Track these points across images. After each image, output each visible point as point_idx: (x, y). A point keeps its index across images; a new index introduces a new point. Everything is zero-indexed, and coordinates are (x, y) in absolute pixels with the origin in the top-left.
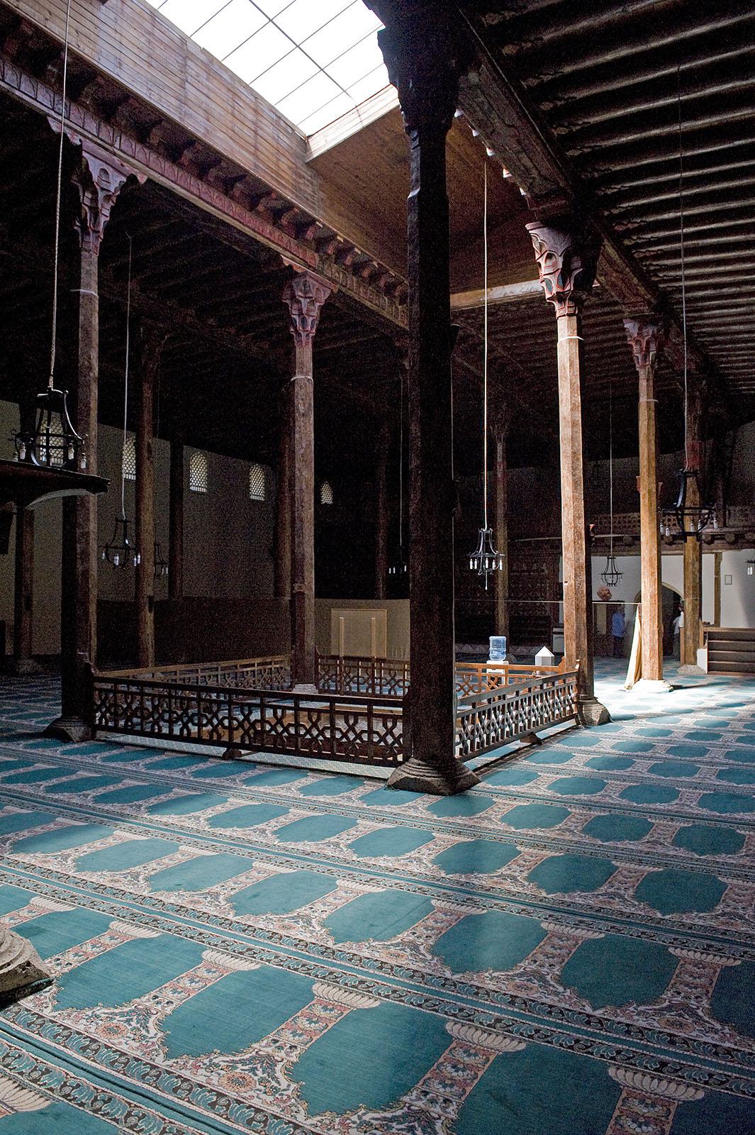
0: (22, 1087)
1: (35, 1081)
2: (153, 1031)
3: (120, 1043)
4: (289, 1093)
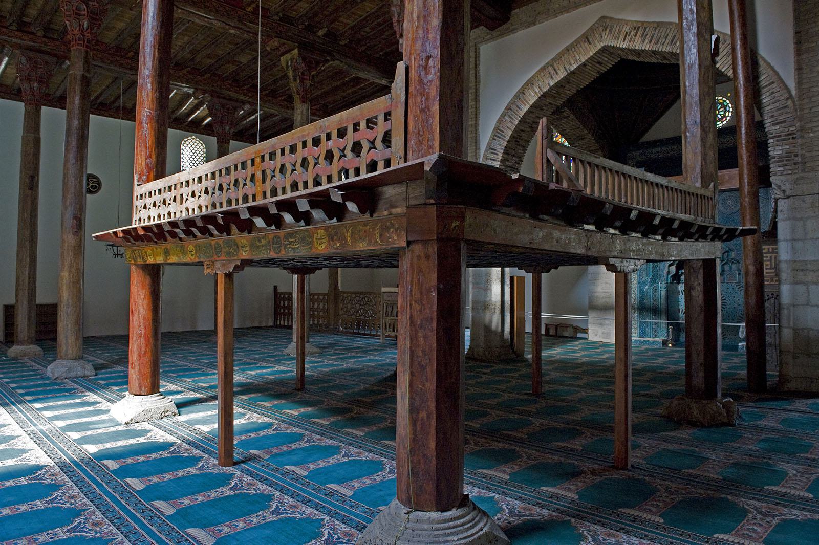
0: (293, 471)
1: (331, 492)
2: (326, 532)
3: (345, 528)
4: (326, 527)
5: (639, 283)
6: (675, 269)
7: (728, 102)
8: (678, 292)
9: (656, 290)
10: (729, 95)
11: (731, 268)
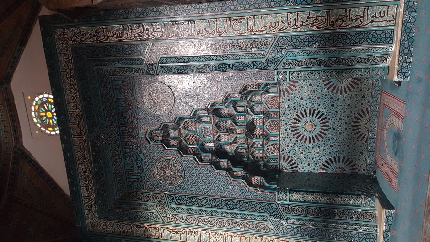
5: (277, 235)
6: (256, 177)
7: (37, 99)
8: (293, 172)
9: (289, 209)
10: (29, 97)
11: (258, 103)
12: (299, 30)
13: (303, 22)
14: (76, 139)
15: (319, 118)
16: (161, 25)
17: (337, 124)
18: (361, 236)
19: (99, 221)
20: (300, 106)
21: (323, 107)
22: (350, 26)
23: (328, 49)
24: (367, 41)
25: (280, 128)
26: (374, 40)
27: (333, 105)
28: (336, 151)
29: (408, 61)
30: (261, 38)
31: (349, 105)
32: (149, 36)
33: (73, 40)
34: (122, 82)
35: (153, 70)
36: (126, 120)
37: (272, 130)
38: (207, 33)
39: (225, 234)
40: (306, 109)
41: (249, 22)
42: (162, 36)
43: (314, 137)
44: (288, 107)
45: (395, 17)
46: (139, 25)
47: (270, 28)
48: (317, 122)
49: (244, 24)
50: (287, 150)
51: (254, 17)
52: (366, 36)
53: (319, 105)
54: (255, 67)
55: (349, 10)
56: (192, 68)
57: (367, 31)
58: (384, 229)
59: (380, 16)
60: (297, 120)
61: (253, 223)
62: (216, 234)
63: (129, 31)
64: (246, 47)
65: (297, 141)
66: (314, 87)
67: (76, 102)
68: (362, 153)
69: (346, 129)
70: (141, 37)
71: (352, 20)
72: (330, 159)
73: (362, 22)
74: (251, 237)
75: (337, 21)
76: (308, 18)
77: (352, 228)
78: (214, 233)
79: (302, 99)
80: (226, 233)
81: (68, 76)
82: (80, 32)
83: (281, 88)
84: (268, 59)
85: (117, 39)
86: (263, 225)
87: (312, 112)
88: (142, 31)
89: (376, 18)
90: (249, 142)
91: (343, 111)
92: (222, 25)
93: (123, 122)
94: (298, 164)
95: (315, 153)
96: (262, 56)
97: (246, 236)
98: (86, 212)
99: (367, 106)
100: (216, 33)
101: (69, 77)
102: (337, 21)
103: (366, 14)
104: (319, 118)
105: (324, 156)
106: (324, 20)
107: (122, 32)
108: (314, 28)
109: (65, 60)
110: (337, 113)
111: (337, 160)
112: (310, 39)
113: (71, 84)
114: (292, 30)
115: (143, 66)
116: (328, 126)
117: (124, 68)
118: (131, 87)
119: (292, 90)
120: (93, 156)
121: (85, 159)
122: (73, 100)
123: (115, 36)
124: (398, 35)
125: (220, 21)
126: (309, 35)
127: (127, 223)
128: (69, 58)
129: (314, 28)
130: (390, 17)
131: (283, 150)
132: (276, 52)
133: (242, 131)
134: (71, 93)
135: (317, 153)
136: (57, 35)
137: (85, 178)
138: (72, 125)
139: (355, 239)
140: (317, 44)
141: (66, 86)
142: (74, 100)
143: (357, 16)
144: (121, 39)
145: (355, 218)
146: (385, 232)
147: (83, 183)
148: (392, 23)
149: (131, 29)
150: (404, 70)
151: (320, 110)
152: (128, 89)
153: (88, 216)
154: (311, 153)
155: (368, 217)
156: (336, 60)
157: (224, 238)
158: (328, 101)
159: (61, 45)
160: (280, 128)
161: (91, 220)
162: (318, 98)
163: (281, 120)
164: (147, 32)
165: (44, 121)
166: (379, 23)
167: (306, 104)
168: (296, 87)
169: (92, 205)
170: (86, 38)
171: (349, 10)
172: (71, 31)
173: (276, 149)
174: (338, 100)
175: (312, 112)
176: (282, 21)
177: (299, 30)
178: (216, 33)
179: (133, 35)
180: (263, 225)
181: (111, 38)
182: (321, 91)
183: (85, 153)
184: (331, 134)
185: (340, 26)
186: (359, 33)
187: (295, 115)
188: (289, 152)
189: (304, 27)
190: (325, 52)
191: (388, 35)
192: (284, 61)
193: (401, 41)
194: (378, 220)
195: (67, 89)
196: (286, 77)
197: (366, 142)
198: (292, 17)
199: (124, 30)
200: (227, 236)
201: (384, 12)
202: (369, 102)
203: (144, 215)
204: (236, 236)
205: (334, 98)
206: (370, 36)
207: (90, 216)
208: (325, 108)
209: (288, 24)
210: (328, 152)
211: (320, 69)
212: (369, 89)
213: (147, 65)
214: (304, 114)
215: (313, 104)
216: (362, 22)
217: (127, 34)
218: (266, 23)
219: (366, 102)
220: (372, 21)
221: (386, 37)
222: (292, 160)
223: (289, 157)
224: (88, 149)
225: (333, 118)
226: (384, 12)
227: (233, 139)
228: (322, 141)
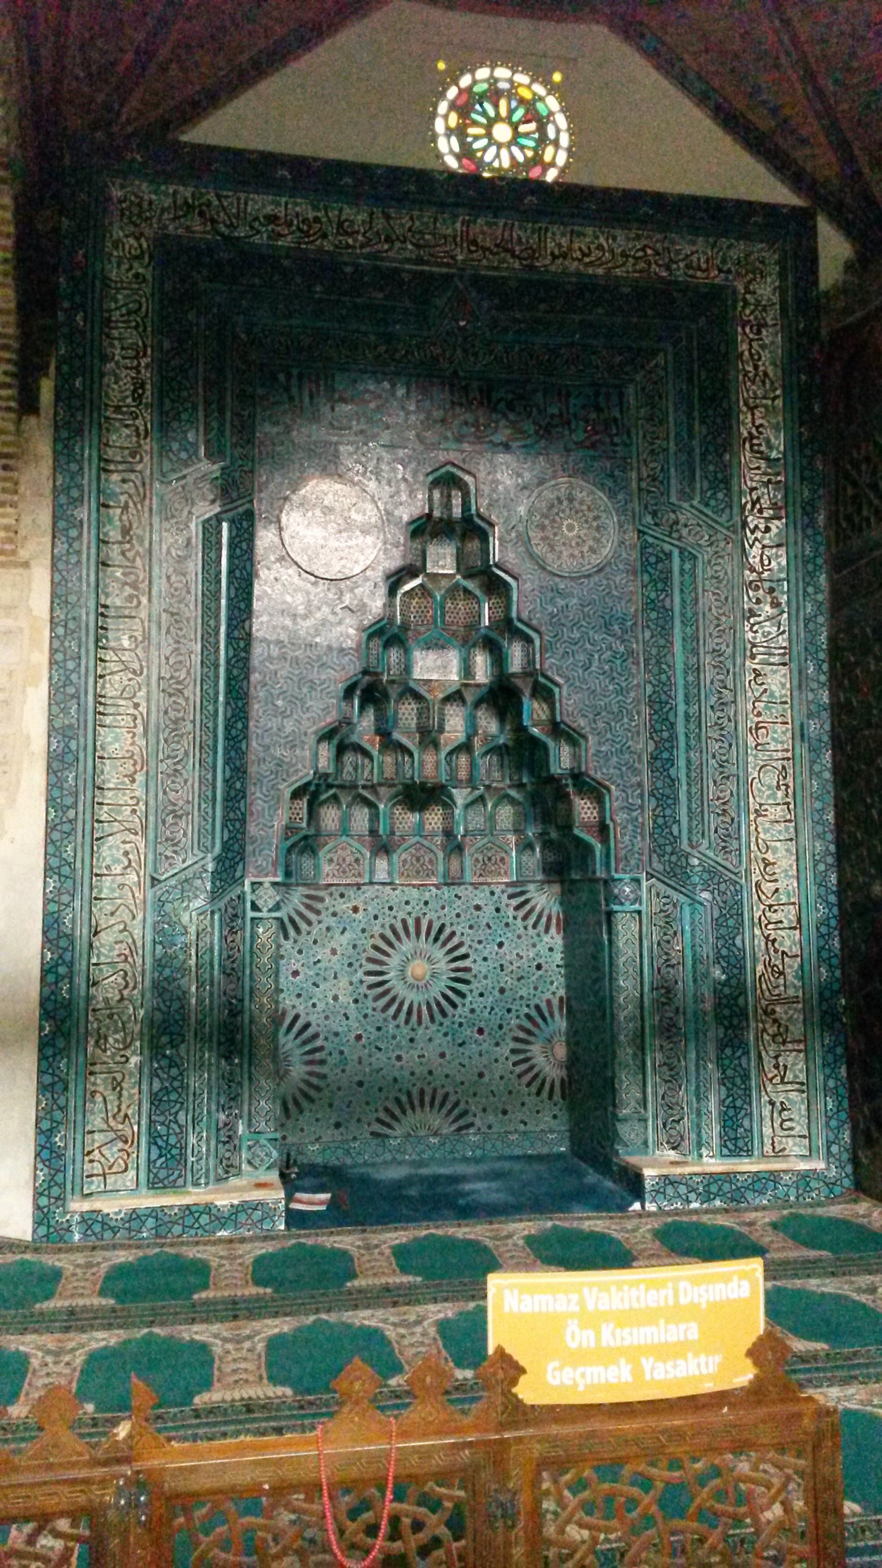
12: (757, 932)
13: (774, 940)
14: (458, 225)
15: (445, 996)
16: (780, 570)
17: (425, 1051)
18: (173, 1140)
19: (147, 231)
20: (480, 942)
21: (474, 1006)
22: (763, 1053)
23: (708, 1006)
24: (160, 1156)
25: (414, 886)
26: (731, 1112)
27: (481, 1031)
28: (342, 1053)
29: (692, 1196)
30: (739, 839)
31: (481, 1075)
32: (752, 532)
33: (748, 296)
34: (615, 420)
35: (656, 524)
36: (502, 405)
37: (405, 861)
38: (757, 694)
39: (136, 706)
40: (471, 959)
41: (779, 808)
42: (752, 570)
43: (386, 986)
44: (478, 908)
45: (780, 1154)
46: (780, 508)
47: (764, 859)
48: (435, 992)
49: (773, 796)
50: (343, 906)
51: (790, 821)
52: (740, 1092)
53: (481, 995)
54: (660, 821)
55: (802, 1047)
56: (662, 642)
57: (750, 1096)
58: (218, 1203)
59: (783, 1121)
60: (438, 935)
61: (188, 802)
62: (134, 672)
63: (765, 474)
64: (719, 798)
65: (372, 936)
66: (534, 978)
67: (574, 259)
68: (338, 1125)
69: (412, 1074)
70: (749, 506)
71: (776, 1057)
72: (316, 1036)
73: (771, 1080)
74: (137, 794)
75: (775, 1021)
76: (783, 952)
77: (198, 1111)
78: (136, 666)
79: (501, 945)
80: (143, 709)
81: (649, 252)
82: (766, 325)
83: (531, 887)
84: (687, 856)
85: (745, 434)
86: (185, 835)
87: (461, 977)
88: (765, 515)
89: (780, 1113)
90: (382, 790)
91: (466, 1062)
92: (773, 739)
93: (495, 396)
94: (295, 941)
95: (334, 992)
96: (695, 839)
97: (140, 778)
98: (186, 192)
99: (478, 1122)
100: (756, 719)
101: (646, 255)
102: (775, 1021)
103: (789, 1087)
104: (445, 996)
105: (327, 1018)
106: (777, 992)
107: (762, 453)
108: (760, 968)
109: (694, 257)
110: (460, 1045)
111: (314, 1056)
112: (734, 961)
113: (627, 256)
114: (757, 915)
115: (673, 500)
116: (420, 1022)
117: (667, 439)
118: (603, 443)
119: (525, 918)
120: (397, 271)
121: (388, 239)
122: (580, 249)
123: (754, 431)
124: (747, 1165)
125: (784, 733)
126: (744, 958)
127: (149, 342)
128: (700, 269)
129: (760, 968)
130: (780, 1142)
131: (342, 896)
132: (706, 876)
133: (429, 770)
134: (600, 247)
135: (335, 998)
136: (762, 250)
137: (317, 220)
138: (505, 225)
139: (163, 1124)
140: (724, 977)
141: (621, 240)
142: (578, 254)
143: (785, 1067)
144: (747, 446)
145: (222, 1117)
146: (208, 1209)
147: (298, 209)
148: (768, 1148)
149: (769, 481)
150: (670, 1191)
151: (469, 998)
152: (597, 433)
153: (166, 194)
154: (335, 977)
155: (227, 1155)
156: (674, 1025)
157: (122, 702)
158: (493, 1017)
159: (734, 254)
160: (414, 886)
161: (151, 203)
162: (502, 991)
163: (437, 887)
164: (762, 527)
165: (481, 105)
166: (768, 1120)
167: (485, 959)
168: (535, 926)
169: (213, 221)
170: (752, 340)
171: (802, 1047)
172: (769, 299)
173: (344, 872)
174: (497, 1044)
175: (461, 977)
176: (777, 890)
177: (757, 932)
178: (756, 719)
179: (754, 484)
180: (185, 835)
181: (749, 416)
182: (522, 998)
183: (410, 247)
184: (397, 1032)
185: (764, 1030)
186: (746, 1077)
187: (454, 928)
188: (334, 914)
189: (763, 944)
190: (698, 999)
191: (740, 1143)
192: (675, 896)
193: (735, 1173)
194: (223, 1185)
195: (614, 238)
196: (627, 903)
197: (372, 1133)
198: (788, 915)
199: (768, 459)
200: (131, 711)
201: (791, 1129)
202: (490, 1127)
203: (184, 416)
204: (133, 744)
205: (501, 1033)
206: (739, 1103)
207: (168, 202)
208: (472, 1011)
209: (770, 906)
210: (340, 1029)
211: (646, 989)
212: (525, 1124)
213: (674, 512)
214: (456, 954)
215: (486, 977)
216: (771, 1080)
217: (758, 468)
218: (775, 851)
219: (491, 1119)
220: (772, 1103)
221: (736, 1143)
222: (309, 923)
223: (318, 912)
224: (420, 261)
225: (446, 1034)
226: (791, 1129)
227: (405, 741)
228: (374, 1009)
